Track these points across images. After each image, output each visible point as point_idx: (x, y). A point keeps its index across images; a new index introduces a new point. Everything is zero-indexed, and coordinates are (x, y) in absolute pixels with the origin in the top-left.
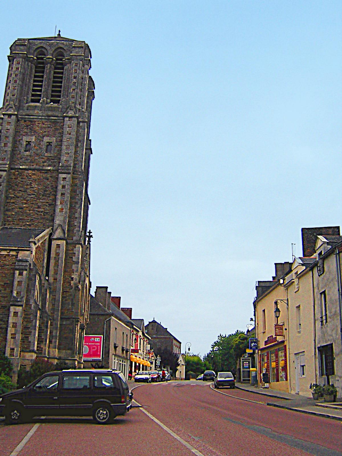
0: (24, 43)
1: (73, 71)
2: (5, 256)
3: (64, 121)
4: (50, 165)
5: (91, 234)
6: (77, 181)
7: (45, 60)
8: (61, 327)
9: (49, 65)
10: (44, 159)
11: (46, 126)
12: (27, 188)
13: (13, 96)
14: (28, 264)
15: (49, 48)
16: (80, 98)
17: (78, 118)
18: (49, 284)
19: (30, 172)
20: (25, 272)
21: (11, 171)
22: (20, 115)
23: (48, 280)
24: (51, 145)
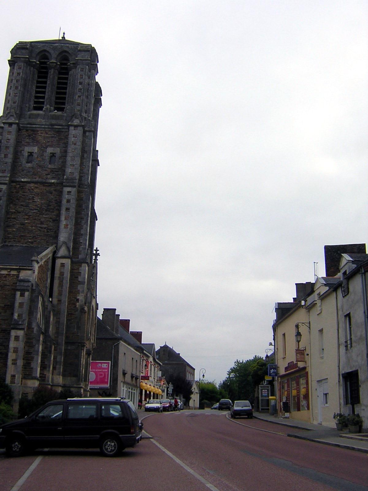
0: (25, 47)
1: (79, 77)
2: (5, 275)
5: (98, 252)
9: (52, 70)
10: (47, 171)
11: (50, 135)
14: (30, 284)
16: (86, 106)
17: (83, 127)
18: (53, 306)
19: (32, 185)
20: (27, 294)
21: (12, 184)
23: (51, 302)
24: (55, 156)
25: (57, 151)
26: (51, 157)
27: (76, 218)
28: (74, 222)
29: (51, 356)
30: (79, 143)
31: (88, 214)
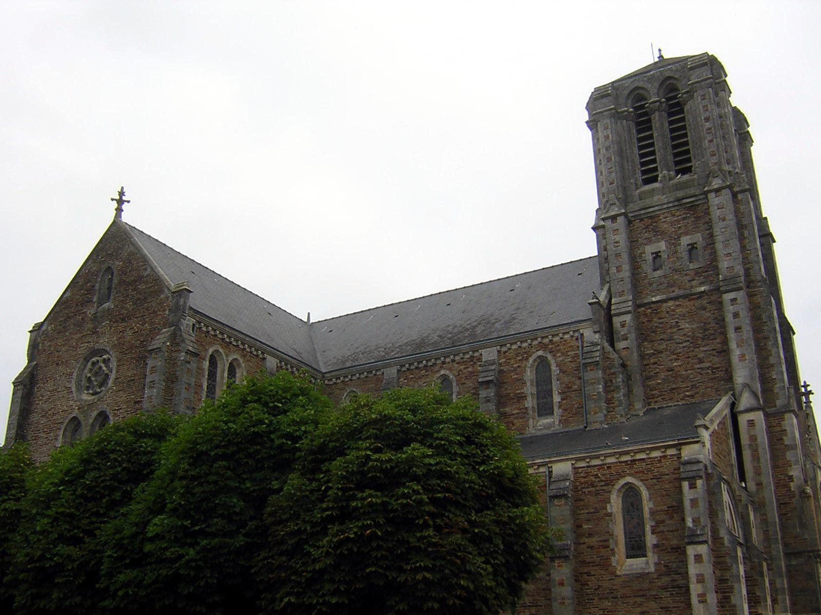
0: (605, 93)
1: (702, 110)
2: (659, 459)
4: (703, 283)
5: (809, 389)
8: (788, 571)
9: (657, 113)
10: (689, 275)
11: (680, 217)
12: (672, 333)
13: (611, 184)
14: (701, 466)
16: (726, 152)
17: (730, 187)
18: (750, 495)
19: (671, 303)
20: (699, 482)
21: (639, 310)
22: (630, 212)
23: (746, 488)
24: (697, 248)
25: (698, 238)
26: (690, 251)
27: (757, 342)
28: (754, 347)
29: (764, 581)
30: (731, 216)
31: (775, 327)
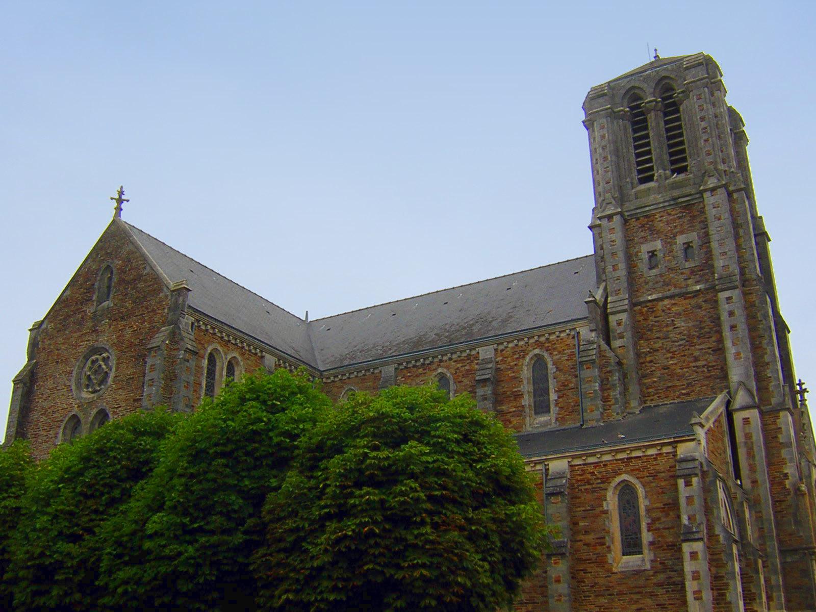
0: (602, 93)
1: (697, 110)
2: (655, 457)
3: (703, 199)
6: (754, 298)
7: (644, 107)
8: (783, 568)
9: (653, 113)
10: (684, 274)
11: (675, 216)
15: (646, 85)
16: (722, 151)
17: (725, 186)
18: (745, 492)
19: (666, 302)
20: (695, 480)
22: (626, 211)
23: (741, 486)
24: (692, 247)
25: (693, 237)
26: (686, 250)
28: (749, 346)
29: (760, 578)
